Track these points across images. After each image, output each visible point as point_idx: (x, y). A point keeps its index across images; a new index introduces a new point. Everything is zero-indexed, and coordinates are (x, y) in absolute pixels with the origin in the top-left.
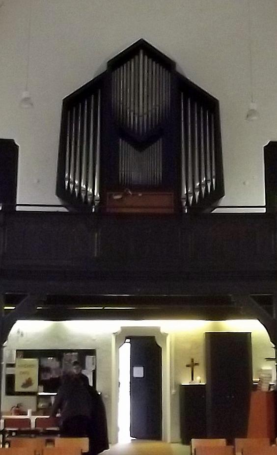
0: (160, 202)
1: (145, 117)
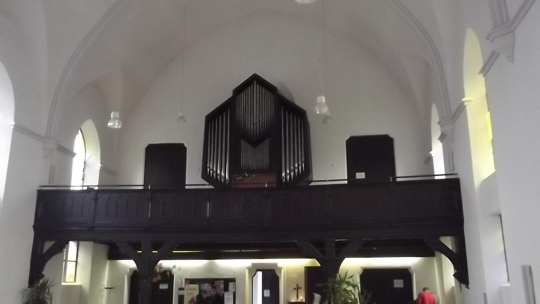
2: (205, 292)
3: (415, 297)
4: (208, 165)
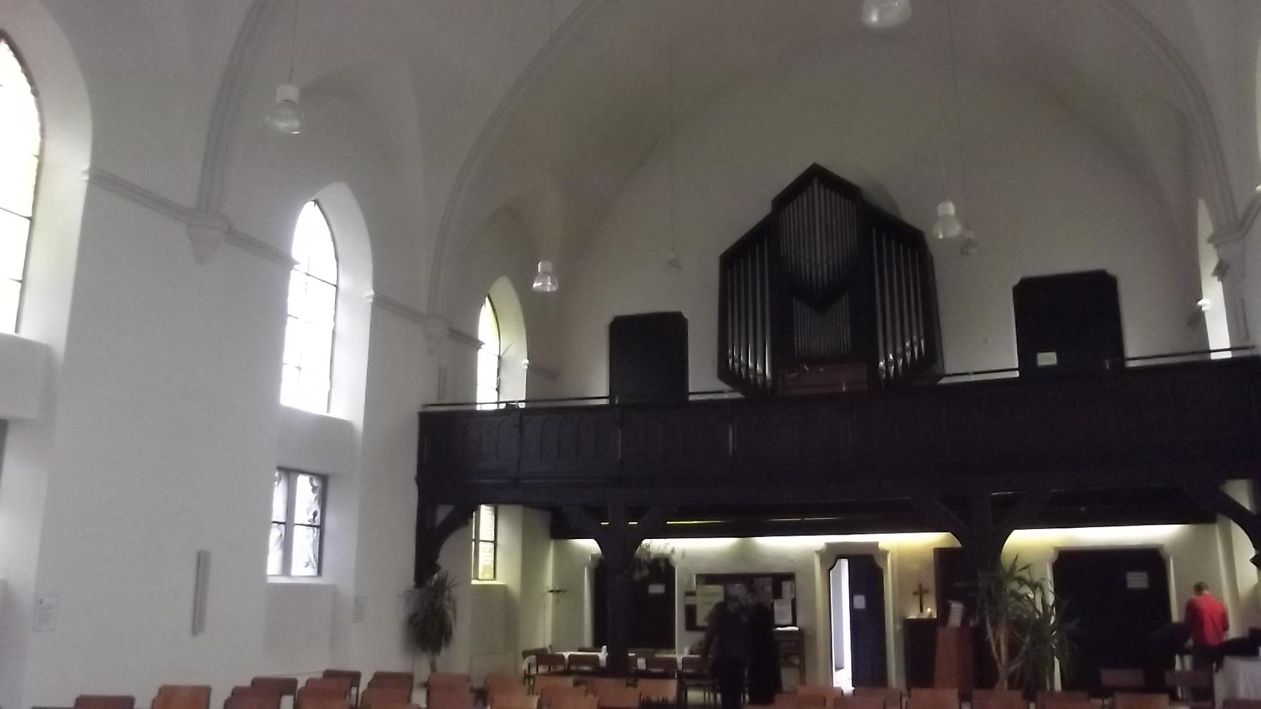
0: (845, 381)
1: (825, 266)
2: (736, 599)
3: (1176, 615)
4: (730, 352)
